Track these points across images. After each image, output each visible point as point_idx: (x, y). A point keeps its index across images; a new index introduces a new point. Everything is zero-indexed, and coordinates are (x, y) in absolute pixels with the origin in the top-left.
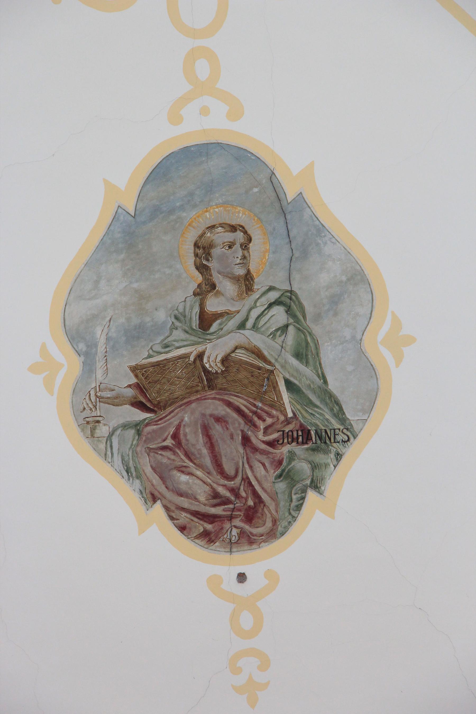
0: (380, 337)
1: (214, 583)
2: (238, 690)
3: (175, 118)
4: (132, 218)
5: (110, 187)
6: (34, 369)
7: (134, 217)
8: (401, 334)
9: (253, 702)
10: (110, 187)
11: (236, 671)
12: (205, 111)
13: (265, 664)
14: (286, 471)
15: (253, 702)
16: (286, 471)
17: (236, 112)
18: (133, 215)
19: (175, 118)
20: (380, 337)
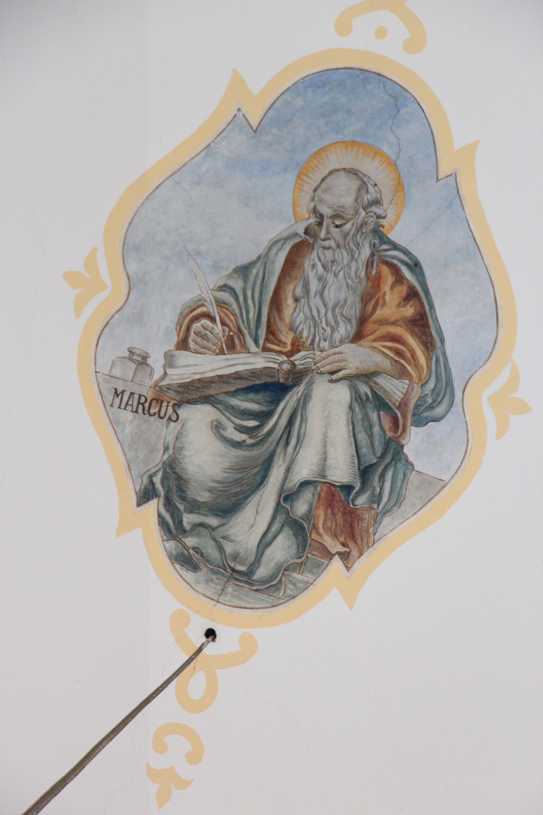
0: (105, 294)
1: (178, 622)
2: (152, 774)
3: (343, 26)
4: (253, 132)
5: (237, 81)
6: (523, 408)
7: (255, 132)
8: (78, 291)
9: (163, 798)
10: (237, 81)
11: (160, 747)
12: (381, 33)
13: (195, 756)
14: (412, 405)
15: (163, 798)
16: (412, 405)
17: (415, 43)
18: (255, 129)
19: (343, 26)
20: (105, 294)
